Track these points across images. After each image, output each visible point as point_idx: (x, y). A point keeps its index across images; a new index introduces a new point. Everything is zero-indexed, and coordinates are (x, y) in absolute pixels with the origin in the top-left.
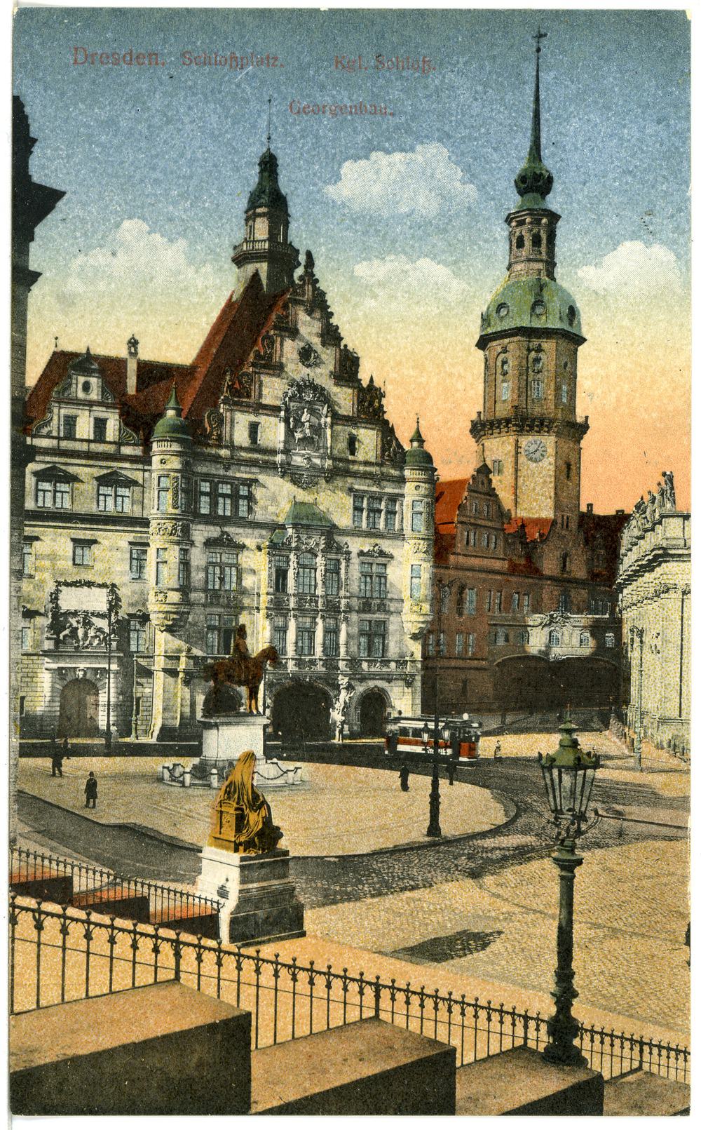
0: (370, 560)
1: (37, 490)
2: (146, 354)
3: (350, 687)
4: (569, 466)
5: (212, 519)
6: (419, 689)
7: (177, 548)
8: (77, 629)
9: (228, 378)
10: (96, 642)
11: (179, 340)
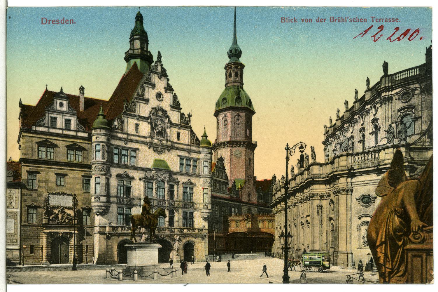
1: (38, 151)
3: (180, 240)
7: (104, 177)
8: (58, 214)
9: (125, 103)
10: (67, 221)
11: (103, 90)
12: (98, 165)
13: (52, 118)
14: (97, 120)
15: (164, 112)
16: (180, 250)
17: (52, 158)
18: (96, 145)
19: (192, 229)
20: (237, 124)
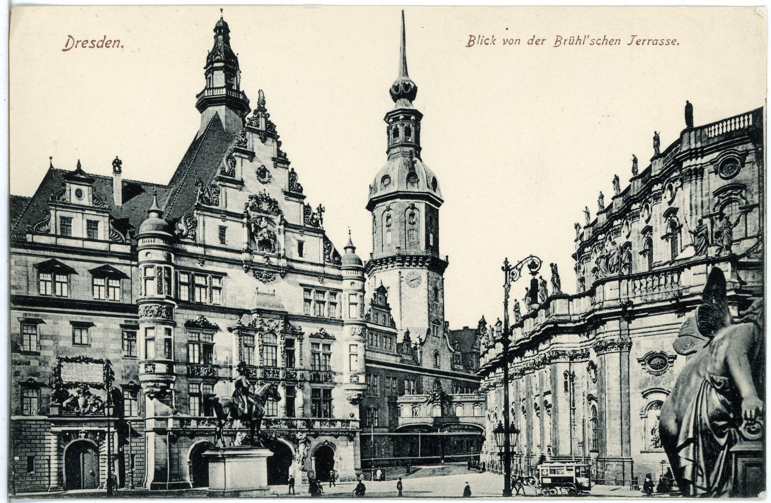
0: (317, 340)
2: (130, 173)
3: (307, 442)
4: (436, 290)
6: (358, 443)
8: (78, 397)
15: (273, 203)
19: (330, 421)
20: (410, 223)
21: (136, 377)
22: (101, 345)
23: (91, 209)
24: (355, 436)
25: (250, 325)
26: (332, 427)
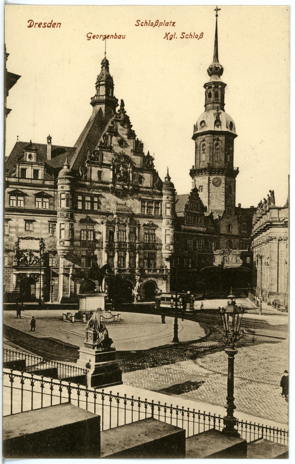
1: (10, 199)
2: (55, 143)
3: (140, 281)
5: (83, 211)
8: (27, 257)
10: (35, 262)
12: (62, 212)
13: (22, 169)
14: (62, 171)
15: (127, 157)
16: (141, 290)
17: (22, 206)
18: (61, 194)
21: (55, 247)
22: (39, 231)
23: (36, 164)
24: (167, 277)
25: (112, 221)
26: (155, 273)
